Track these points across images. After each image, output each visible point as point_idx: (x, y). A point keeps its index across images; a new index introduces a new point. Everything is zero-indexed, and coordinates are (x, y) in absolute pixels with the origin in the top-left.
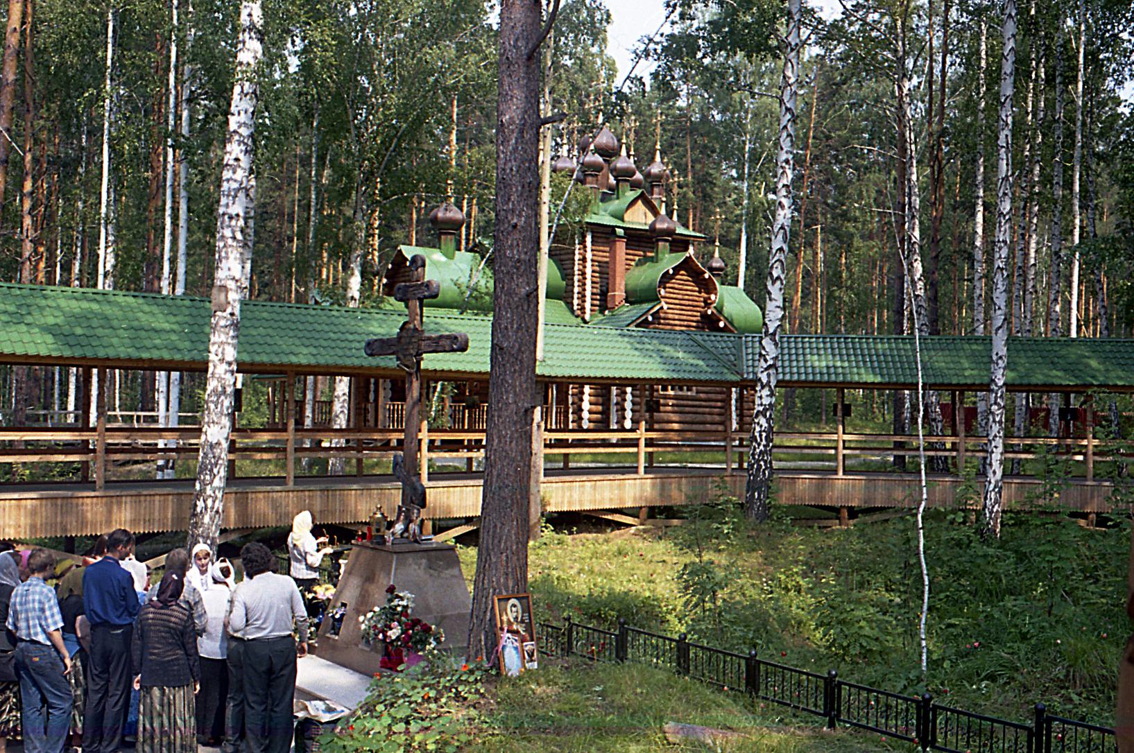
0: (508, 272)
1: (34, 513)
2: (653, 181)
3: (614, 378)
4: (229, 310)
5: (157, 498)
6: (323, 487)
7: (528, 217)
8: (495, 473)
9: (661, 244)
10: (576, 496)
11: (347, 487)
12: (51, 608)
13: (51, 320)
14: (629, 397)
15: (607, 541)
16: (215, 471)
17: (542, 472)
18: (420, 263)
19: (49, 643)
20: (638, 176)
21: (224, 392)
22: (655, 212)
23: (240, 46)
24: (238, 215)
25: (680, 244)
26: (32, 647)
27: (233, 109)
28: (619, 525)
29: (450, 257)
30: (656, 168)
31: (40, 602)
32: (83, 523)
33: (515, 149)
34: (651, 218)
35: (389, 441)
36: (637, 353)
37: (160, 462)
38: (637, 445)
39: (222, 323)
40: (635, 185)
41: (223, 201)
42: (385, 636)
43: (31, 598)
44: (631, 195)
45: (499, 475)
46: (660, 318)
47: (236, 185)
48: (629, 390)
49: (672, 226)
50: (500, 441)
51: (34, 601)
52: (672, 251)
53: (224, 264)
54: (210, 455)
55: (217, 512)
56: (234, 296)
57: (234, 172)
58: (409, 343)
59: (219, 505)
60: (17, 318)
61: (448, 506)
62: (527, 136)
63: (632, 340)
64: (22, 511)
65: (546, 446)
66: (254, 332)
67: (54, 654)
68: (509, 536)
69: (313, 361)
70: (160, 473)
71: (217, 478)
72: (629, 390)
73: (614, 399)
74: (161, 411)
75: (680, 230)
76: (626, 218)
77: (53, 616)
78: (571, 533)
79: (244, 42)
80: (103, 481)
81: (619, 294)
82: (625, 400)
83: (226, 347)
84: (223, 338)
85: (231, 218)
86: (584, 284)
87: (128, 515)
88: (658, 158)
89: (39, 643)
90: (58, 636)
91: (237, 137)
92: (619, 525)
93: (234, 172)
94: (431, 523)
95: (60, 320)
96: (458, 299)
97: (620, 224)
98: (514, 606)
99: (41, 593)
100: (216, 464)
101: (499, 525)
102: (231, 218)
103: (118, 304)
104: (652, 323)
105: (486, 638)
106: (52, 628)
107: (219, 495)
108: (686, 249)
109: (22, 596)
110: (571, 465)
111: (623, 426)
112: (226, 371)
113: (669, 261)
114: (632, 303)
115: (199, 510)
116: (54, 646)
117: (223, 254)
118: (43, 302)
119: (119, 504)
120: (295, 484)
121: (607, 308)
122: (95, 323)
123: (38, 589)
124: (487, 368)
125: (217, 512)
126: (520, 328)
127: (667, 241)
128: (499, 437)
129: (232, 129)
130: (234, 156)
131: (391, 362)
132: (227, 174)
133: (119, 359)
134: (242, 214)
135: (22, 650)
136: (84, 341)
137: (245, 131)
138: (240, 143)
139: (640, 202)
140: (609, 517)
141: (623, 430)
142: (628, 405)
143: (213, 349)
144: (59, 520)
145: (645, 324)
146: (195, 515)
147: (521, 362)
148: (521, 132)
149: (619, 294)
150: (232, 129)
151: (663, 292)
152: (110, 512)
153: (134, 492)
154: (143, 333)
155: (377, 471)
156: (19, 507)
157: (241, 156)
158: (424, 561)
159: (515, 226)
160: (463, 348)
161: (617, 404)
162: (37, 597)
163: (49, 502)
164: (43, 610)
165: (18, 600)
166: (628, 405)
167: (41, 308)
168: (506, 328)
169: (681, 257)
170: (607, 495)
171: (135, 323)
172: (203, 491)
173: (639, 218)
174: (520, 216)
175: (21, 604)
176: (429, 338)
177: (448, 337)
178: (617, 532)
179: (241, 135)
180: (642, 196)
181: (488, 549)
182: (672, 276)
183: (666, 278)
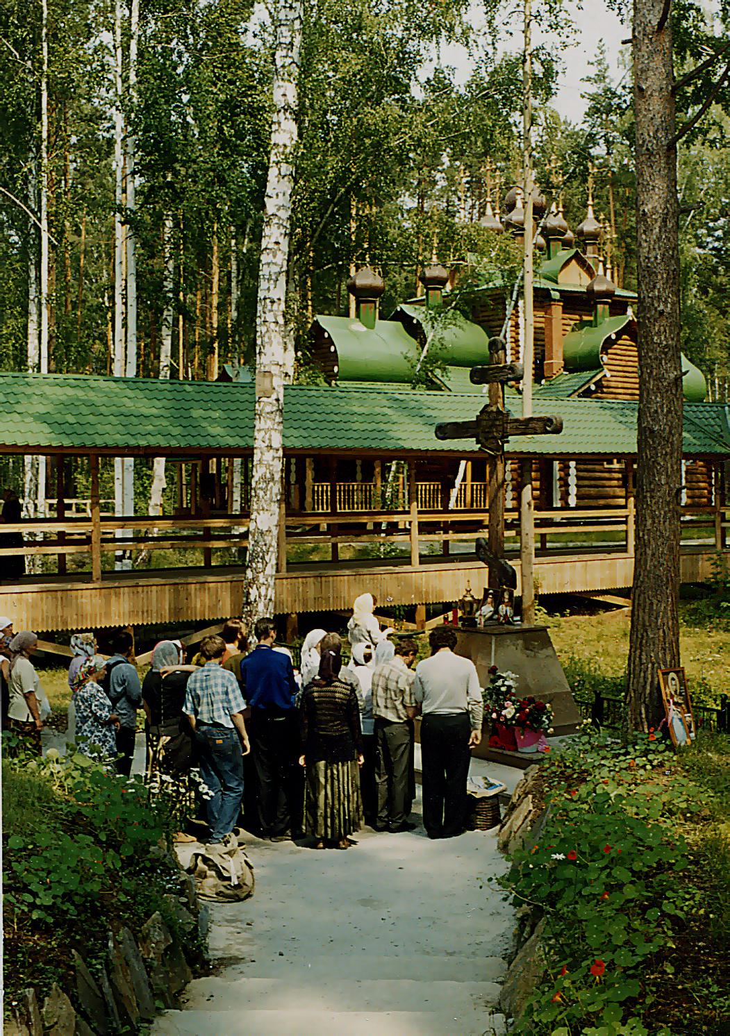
0: (656, 358)
1: (34, 606)
2: (585, 239)
3: (465, 452)
4: (274, 396)
5: (154, 588)
6: (317, 573)
7: (673, 304)
8: (649, 552)
11: (340, 572)
12: (233, 691)
14: (573, 471)
16: (267, 558)
17: (533, 552)
18: (500, 346)
21: (273, 479)
22: (590, 272)
23: (274, 127)
24: (279, 299)
25: (618, 307)
26: (214, 730)
27: (269, 191)
28: (608, 607)
29: (371, 326)
30: (590, 225)
31: (223, 685)
32: (81, 616)
33: (659, 239)
34: (586, 281)
35: (318, 525)
36: (623, 427)
37: (119, 553)
38: (626, 523)
39: (268, 409)
40: (567, 244)
42: (499, 715)
43: (212, 682)
44: (564, 254)
45: (653, 555)
47: (277, 269)
48: (572, 464)
49: (611, 288)
51: (216, 685)
52: (612, 314)
53: (267, 350)
54: (262, 543)
55: (270, 600)
56: (279, 382)
57: (274, 256)
58: (494, 425)
59: (271, 593)
60: (8, 407)
61: (441, 591)
62: (670, 225)
63: (614, 413)
65: (537, 526)
67: (236, 736)
68: (665, 612)
72: (572, 464)
73: (557, 474)
74: (118, 501)
75: (619, 292)
79: (279, 123)
81: (557, 361)
82: (568, 475)
83: (273, 432)
84: (269, 424)
85: (273, 302)
87: (126, 606)
88: (590, 214)
89: (222, 725)
90: (240, 720)
91: (275, 220)
92: (608, 607)
93: (274, 256)
94: (424, 607)
95: (50, 408)
96: (408, 372)
97: (556, 287)
98: (673, 679)
99: (223, 677)
101: (655, 601)
104: (595, 392)
106: (235, 711)
107: (271, 582)
108: (624, 312)
109: (202, 681)
111: (567, 503)
113: (610, 326)
114: (571, 372)
115: (252, 598)
116: (236, 728)
117: (266, 339)
118: (29, 391)
119: (118, 595)
120: (288, 571)
121: (544, 377)
122: (85, 410)
123: (219, 673)
125: (270, 600)
126: (669, 411)
128: (653, 518)
129: (270, 213)
130: (273, 240)
131: (470, 444)
132: (265, 258)
134: (283, 299)
136: (79, 429)
137: (284, 214)
139: (574, 261)
140: (600, 598)
141: (566, 507)
142: (572, 480)
145: (587, 393)
146: (248, 604)
147: (672, 444)
148: (664, 221)
149: (557, 361)
150: (270, 213)
151: (605, 358)
152: (108, 603)
155: (315, 558)
157: (281, 240)
158: (520, 642)
159: (661, 313)
160: (558, 430)
161: (560, 479)
162: (219, 681)
166: (572, 480)
167: (29, 396)
168: (656, 412)
171: (123, 410)
173: (574, 279)
174: (666, 302)
175: (202, 689)
176: (517, 421)
179: (280, 218)
180: (576, 256)
181: (644, 625)
182: (615, 342)
183: (609, 343)
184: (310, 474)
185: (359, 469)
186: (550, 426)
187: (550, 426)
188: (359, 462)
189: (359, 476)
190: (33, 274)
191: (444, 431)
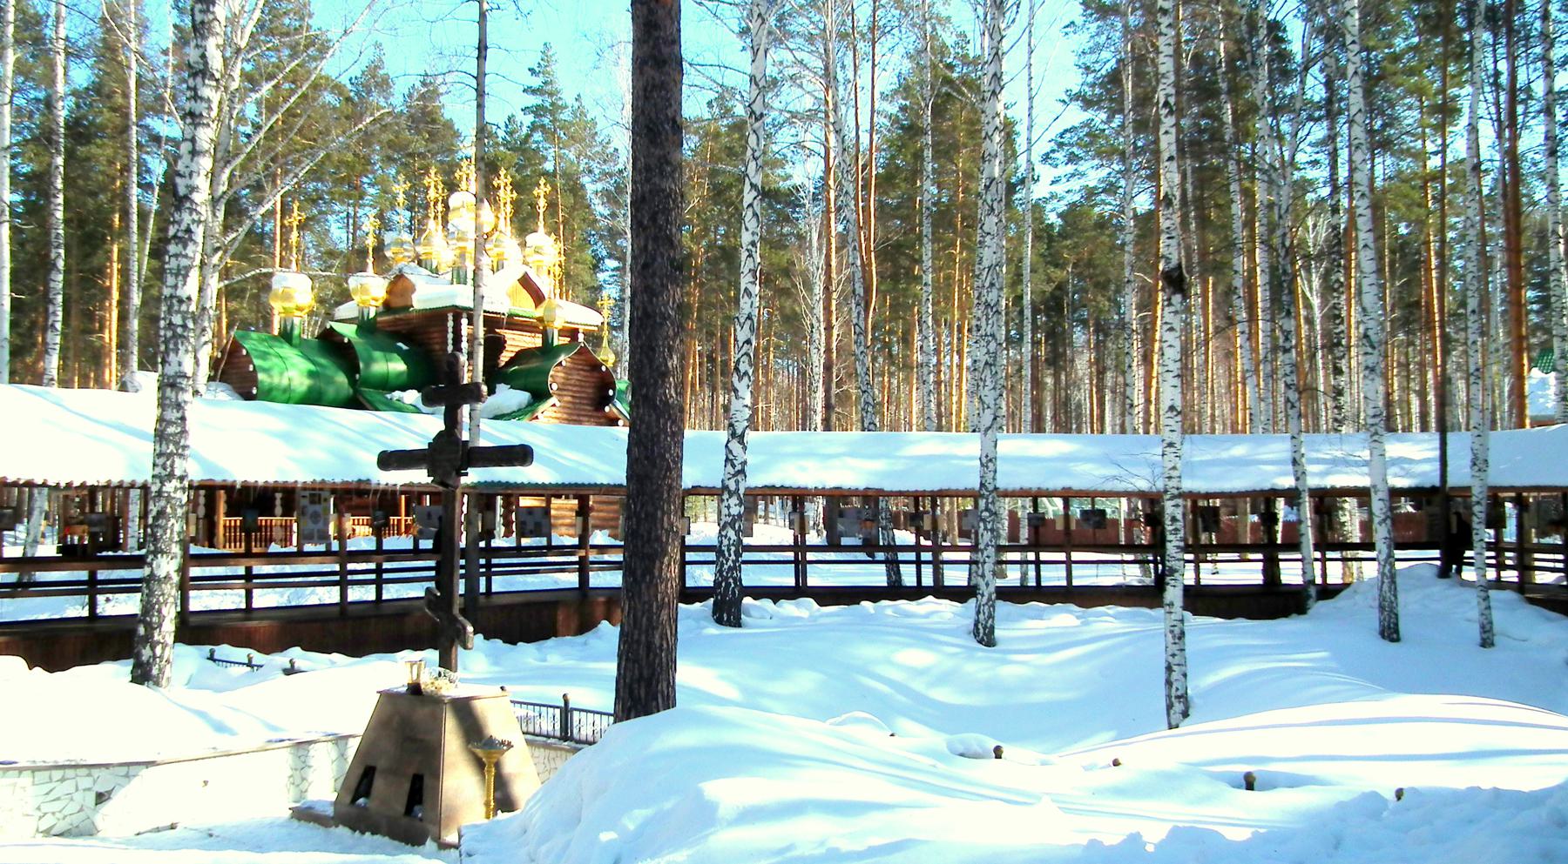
57: (185, 247)
141: (186, 585)
184: (222, 507)
185: (278, 502)
186: (521, 455)
187: (521, 455)
188: (279, 496)
189: (278, 510)
190: (135, 324)
191: (389, 460)
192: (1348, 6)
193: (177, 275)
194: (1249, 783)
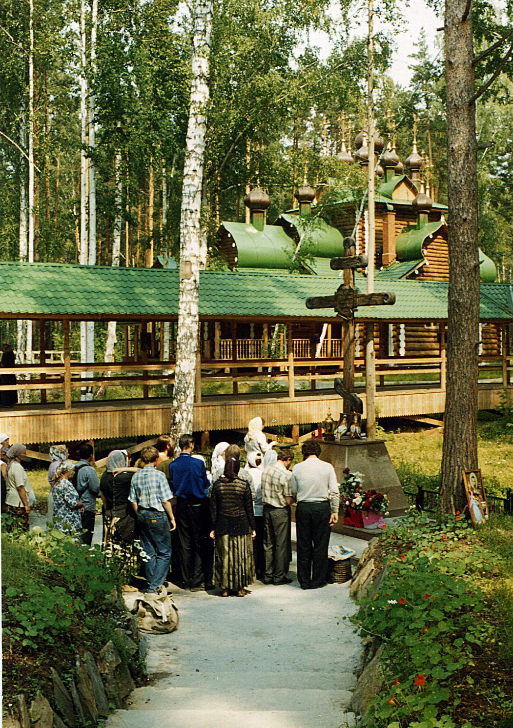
0: (461, 252)
1: (24, 426)
2: (415, 168)
4: (193, 279)
6: (222, 403)
7: (473, 214)
8: (456, 388)
9: (421, 216)
10: (399, 406)
13: (30, 288)
14: (402, 331)
15: (422, 438)
16: (188, 392)
19: (163, 510)
20: (400, 165)
21: (191, 336)
22: (414, 191)
23: (193, 89)
24: (196, 210)
25: (434, 215)
26: (151, 513)
27: (189, 134)
28: (427, 426)
30: (414, 158)
31: (157, 482)
33: (463, 168)
36: (438, 300)
37: (84, 389)
38: (439, 367)
39: (188, 287)
40: (398, 172)
41: (185, 200)
42: (351, 502)
45: (459, 390)
46: (424, 272)
47: (194, 189)
48: (402, 326)
50: (459, 367)
51: (152, 481)
52: (430, 221)
53: (188, 246)
54: (184, 382)
56: (196, 268)
57: (193, 180)
58: (347, 299)
59: (190, 417)
60: (5, 286)
61: (310, 415)
62: (471, 158)
63: (432, 290)
64: (17, 425)
65: (377, 369)
66: (169, 292)
67: (166, 517)
68: (467, 430)
69: (215, 312)
70: (83, 396)
71: (189, 397)
72: (402, 326)
73: (392, 333)
74: (83, 352)
75: (435, 205)
76: (393, 197)
77: (165, 491)
78: (396, 433)
79: (196, 87)
80: (70, 402)
81: (391, 254)
84: (189, 298)
85: (192, 212)
86: (364, 248)
88: (415, 151)
89: (155, 510)
91: (194, 155)
92: (427, 426)
93: (193, 180)
95: (35, 287)
98: (473, 477)
100: (188, 388)
101: (460, 423)
102: (192, 212)
103: (71, 274)
104: (418, 275)
105: (455, 500)
106: (165, 500)
108: (439, 219)
109: (142, 478)
110: (386, 383)
111: (399, 354)
112: (192, 322)
113: (428, 229)
114: (401, 261)
115: (177, 420)
116: (166, 511)
117: (187, 238)
118: (20, 274)
120: (202, 401)
121: (382, 265)
122: (59, 288)
123: (154, 473)
124: (447, 316)
125: (190, 421)
126: (470, 289)
127: (426, 213)
128: (459, 364)
131: (330, 312)
132: (186, 181)
133: (82, 314)
134: (199, 210)
135: (143, 515)
136: (55, 301)
137: (200, 151)
138: (196, 158)
139: (403, 184)
141: (398, 356)
142: (402, 338)
143: (181, 306)
144: (42, 431)
145: (413, 276)
146: (174, 424)
147: (472, 312)
148: (467, 155)
151: (425, 252)
152: (76, 424)
153: (121, 408)
154: (94, 295)
155: (222, 392)
156: (14, 422)
157: (197, 168)
158: (366, 451)
159: (465, 220)
160: (392, 303)
161: (394, 337)
162: (154, 479)
163: (35, 418)
164: (159, 487)
165: (139, 481)
166: (402, 338)
167: (20, 279)
168: (461, 289)
169: (436, 226)
170: (420, 404)
171: (86, 288)
172: (179, 407)
173: (403, 196)
174: (468, 212)
175: (142, 484)
176: (363, 296)
177: (379, 295)
178: (427, 431)
179: (197, 153)
180: (405, 180)
181: (453, 439)
182: (432, 240)
183: (428, 241)
184: (218, 333)
186: (387, 299)
187: (387, 299)
188: (252, 325)
189: (252, 335)
191: (312, 303)
192: (219, 2)
193: (189, 197)
194: (257, 634)
